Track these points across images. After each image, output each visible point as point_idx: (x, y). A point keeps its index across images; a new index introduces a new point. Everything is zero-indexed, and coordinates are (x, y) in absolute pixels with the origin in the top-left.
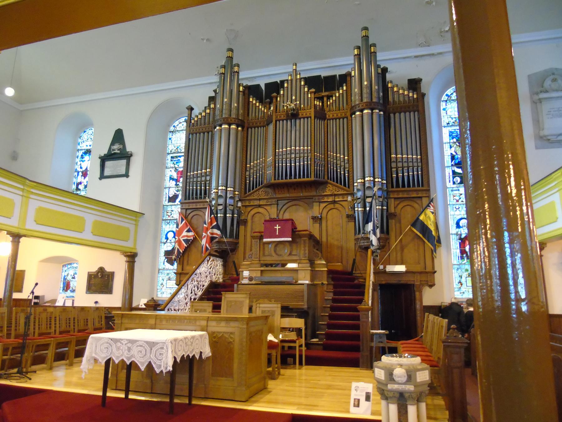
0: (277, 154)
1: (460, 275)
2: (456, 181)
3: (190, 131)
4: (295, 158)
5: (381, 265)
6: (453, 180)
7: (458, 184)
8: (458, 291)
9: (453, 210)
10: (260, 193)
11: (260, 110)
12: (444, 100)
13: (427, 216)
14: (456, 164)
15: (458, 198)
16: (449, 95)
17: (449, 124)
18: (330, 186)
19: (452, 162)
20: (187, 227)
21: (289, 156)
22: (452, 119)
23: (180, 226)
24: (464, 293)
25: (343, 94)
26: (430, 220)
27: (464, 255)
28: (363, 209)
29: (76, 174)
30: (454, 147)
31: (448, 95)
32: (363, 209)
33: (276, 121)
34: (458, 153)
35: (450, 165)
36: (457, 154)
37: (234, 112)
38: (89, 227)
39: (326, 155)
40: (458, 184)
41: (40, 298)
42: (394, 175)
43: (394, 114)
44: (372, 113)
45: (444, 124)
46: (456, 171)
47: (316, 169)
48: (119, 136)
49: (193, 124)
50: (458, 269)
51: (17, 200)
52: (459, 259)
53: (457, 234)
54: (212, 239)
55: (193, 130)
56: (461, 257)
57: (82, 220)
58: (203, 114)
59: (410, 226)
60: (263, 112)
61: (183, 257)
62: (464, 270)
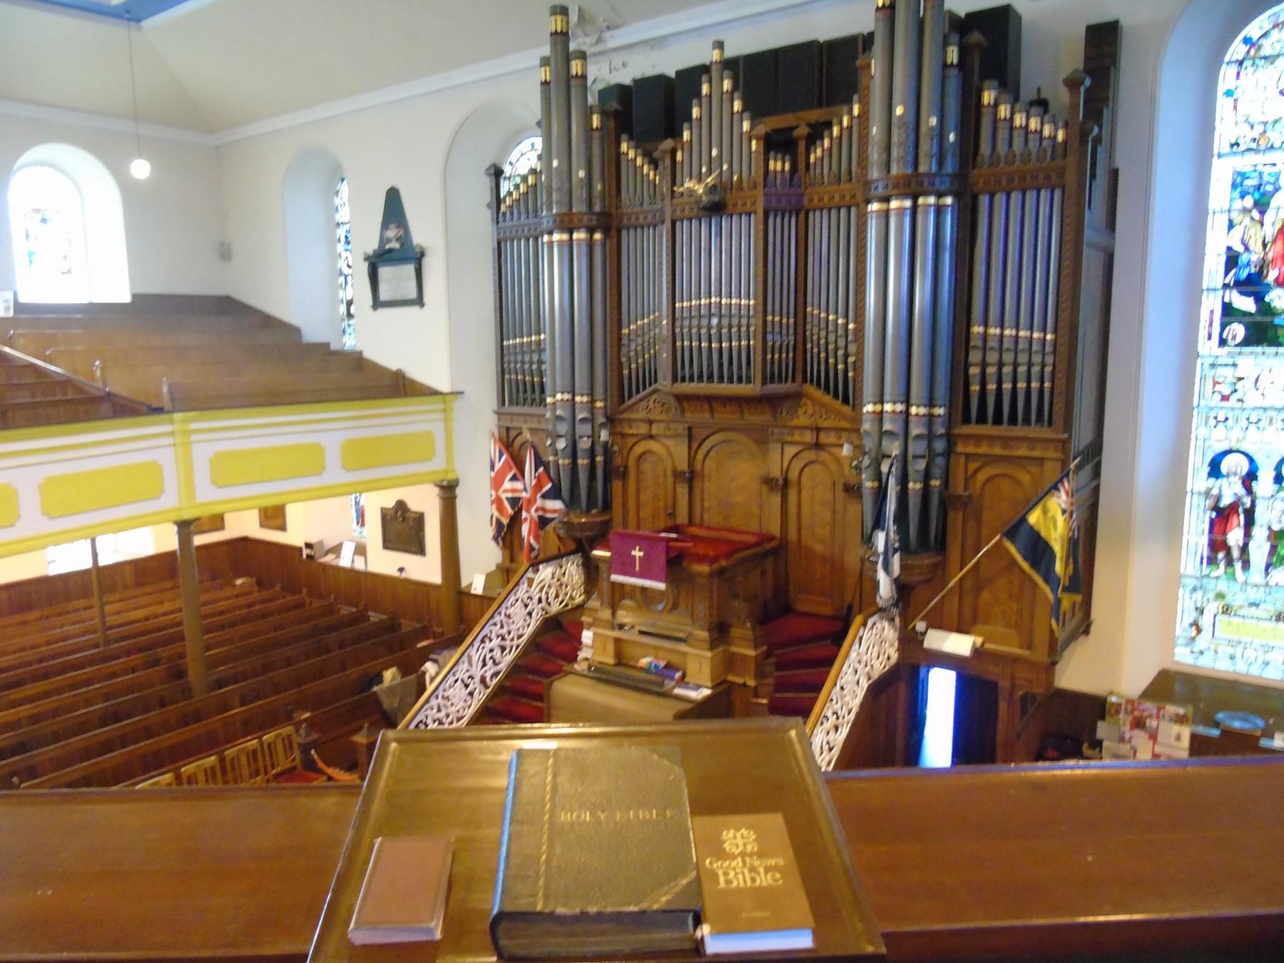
0: (677, 315)
1: (1199, 605)
2: (1230, 338)
3: (499, 234)
4: (720, 327)
5: (922, 619)
6: (1221, 334)
7: (1237, 345)
8: (1187, 645)
9: (1206, 423)
10: (651, 405)
11: (645, 178)
12: (1234, 59)
13: (1050, 515)
14: (1239, 285)
15: (1227, 391)
16: (1255, 39)
17: (1237, 144)
18: (809, 403)
19: (1227, 273)
20: (511, 470)
21: (704, 322)
22: (1252, 127)
23: (498, 466)
24: (1202, 653)
25: (850, 128)
26: (1055, 528)
27: (1221, 555)
28: (876, 484)
29: (342, 279)
30: (1243, 224)
31: (1250, 39)
32: (876, 484)
33: (673, 223)
34: (1252, 247)
35: (1220, 285)
36: (1247, 249)
37: (579, 194)
38: (333, 458)
39: (800, 315)
40: (1242, 344)
41: (315, 547)
42: (975, 388)
43: (992, 196)
44: (915, 208)
45: (1221, 142)
46: (1235, 305)
47: (769, 361)
48: (394, 208)
49: (504, 214)
50: (1194, 589)
51: (166, 457)
52: (1202, 563)
53: (1207, 493)
54: (543, 522)
55: (505, 233)
56: (1209, 558)
57: (317, 452)
58: (522, 188)
59: (998, 537)
60: (652, 185)
61: (512, 534)
62: (1211, 595)
